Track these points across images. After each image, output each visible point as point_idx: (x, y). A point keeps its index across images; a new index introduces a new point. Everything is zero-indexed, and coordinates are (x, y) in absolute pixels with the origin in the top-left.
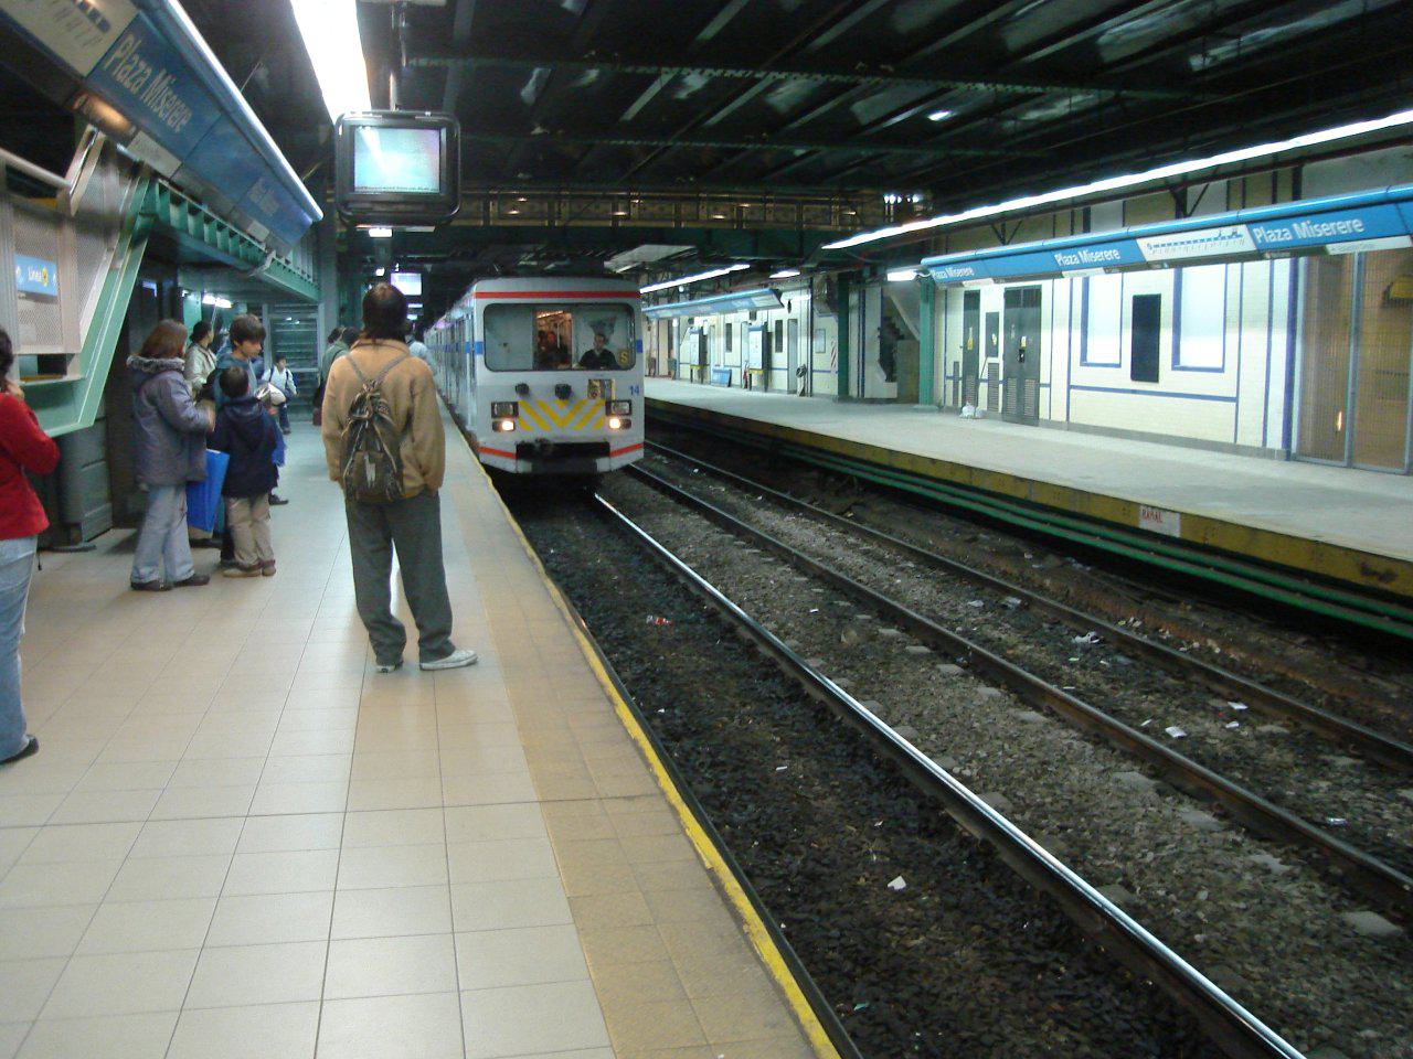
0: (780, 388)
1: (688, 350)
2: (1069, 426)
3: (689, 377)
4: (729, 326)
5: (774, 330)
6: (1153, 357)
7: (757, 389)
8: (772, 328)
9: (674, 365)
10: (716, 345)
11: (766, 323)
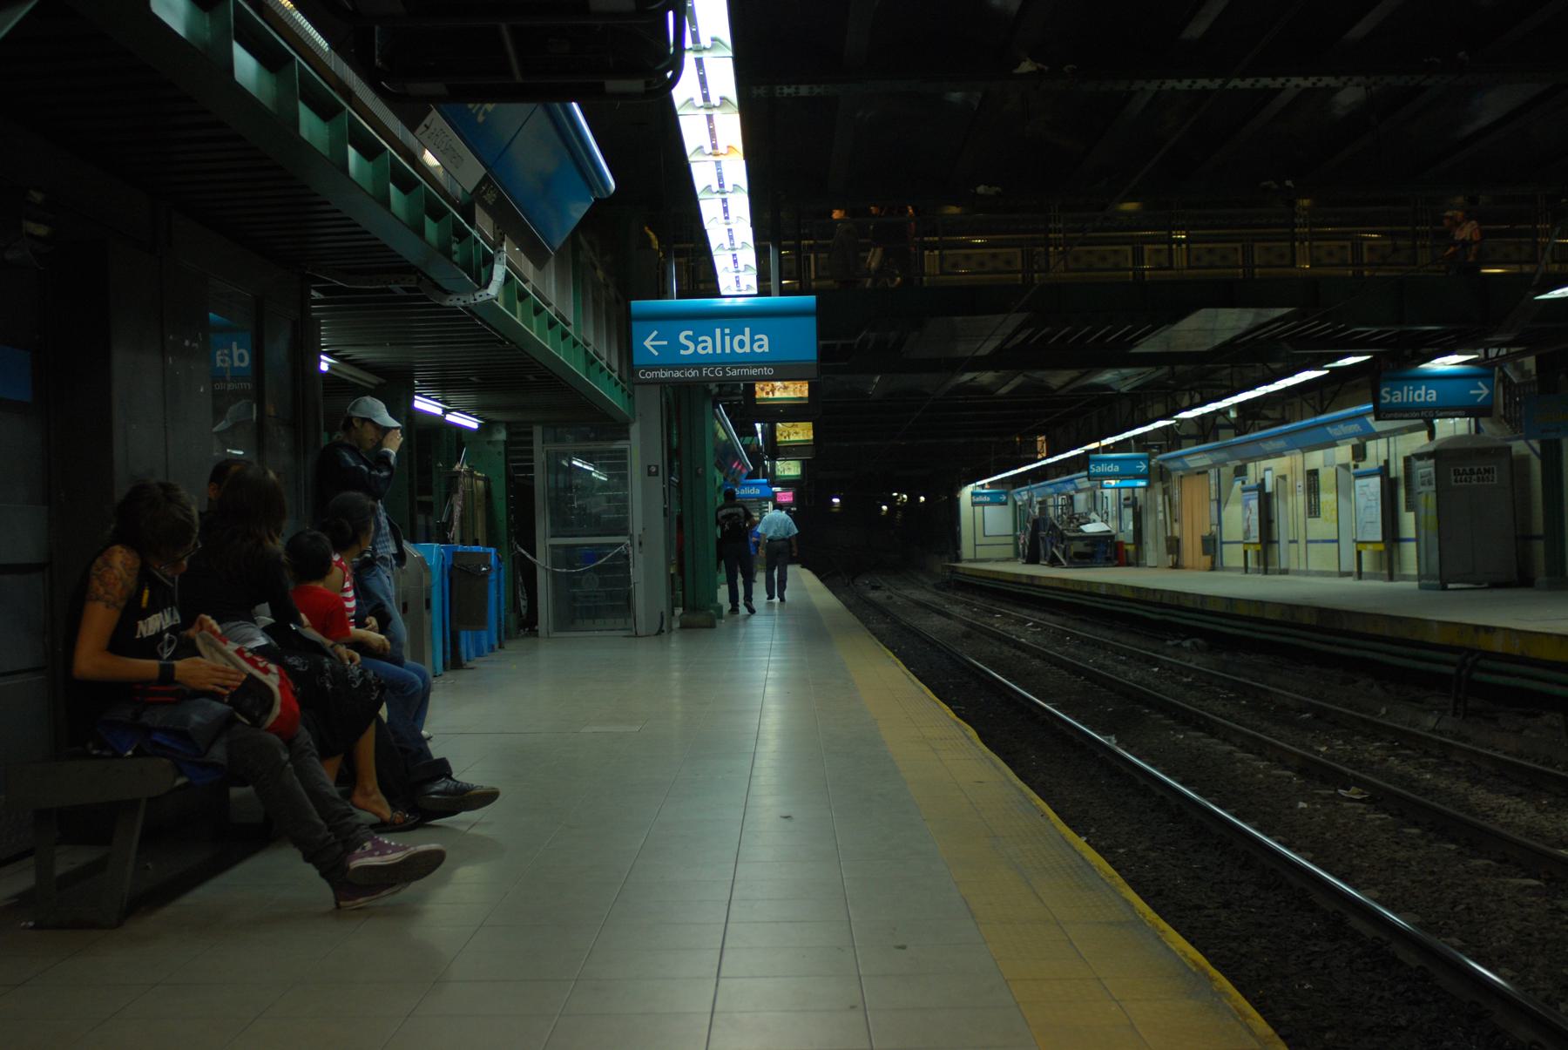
0: (1232, 564)
1: (1239, 517)
2: (1307, 573)
3: (1242, 564)
4: (1313, 474)
5: (1401, 474)
6: (1307, 508)
7: (1373, 576)
8: (1397, 469)
9: (1211, 545)
10: (1291, 508)
11: (1387, 462)
